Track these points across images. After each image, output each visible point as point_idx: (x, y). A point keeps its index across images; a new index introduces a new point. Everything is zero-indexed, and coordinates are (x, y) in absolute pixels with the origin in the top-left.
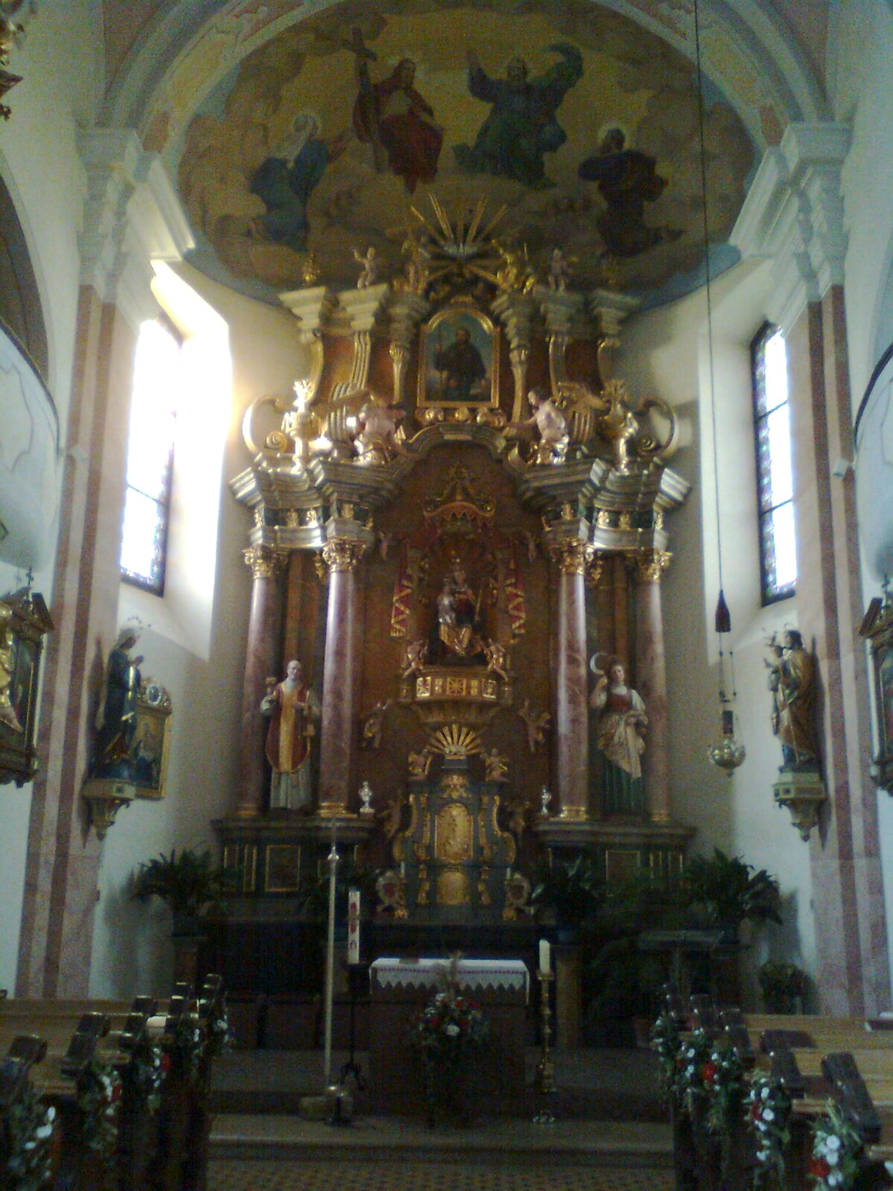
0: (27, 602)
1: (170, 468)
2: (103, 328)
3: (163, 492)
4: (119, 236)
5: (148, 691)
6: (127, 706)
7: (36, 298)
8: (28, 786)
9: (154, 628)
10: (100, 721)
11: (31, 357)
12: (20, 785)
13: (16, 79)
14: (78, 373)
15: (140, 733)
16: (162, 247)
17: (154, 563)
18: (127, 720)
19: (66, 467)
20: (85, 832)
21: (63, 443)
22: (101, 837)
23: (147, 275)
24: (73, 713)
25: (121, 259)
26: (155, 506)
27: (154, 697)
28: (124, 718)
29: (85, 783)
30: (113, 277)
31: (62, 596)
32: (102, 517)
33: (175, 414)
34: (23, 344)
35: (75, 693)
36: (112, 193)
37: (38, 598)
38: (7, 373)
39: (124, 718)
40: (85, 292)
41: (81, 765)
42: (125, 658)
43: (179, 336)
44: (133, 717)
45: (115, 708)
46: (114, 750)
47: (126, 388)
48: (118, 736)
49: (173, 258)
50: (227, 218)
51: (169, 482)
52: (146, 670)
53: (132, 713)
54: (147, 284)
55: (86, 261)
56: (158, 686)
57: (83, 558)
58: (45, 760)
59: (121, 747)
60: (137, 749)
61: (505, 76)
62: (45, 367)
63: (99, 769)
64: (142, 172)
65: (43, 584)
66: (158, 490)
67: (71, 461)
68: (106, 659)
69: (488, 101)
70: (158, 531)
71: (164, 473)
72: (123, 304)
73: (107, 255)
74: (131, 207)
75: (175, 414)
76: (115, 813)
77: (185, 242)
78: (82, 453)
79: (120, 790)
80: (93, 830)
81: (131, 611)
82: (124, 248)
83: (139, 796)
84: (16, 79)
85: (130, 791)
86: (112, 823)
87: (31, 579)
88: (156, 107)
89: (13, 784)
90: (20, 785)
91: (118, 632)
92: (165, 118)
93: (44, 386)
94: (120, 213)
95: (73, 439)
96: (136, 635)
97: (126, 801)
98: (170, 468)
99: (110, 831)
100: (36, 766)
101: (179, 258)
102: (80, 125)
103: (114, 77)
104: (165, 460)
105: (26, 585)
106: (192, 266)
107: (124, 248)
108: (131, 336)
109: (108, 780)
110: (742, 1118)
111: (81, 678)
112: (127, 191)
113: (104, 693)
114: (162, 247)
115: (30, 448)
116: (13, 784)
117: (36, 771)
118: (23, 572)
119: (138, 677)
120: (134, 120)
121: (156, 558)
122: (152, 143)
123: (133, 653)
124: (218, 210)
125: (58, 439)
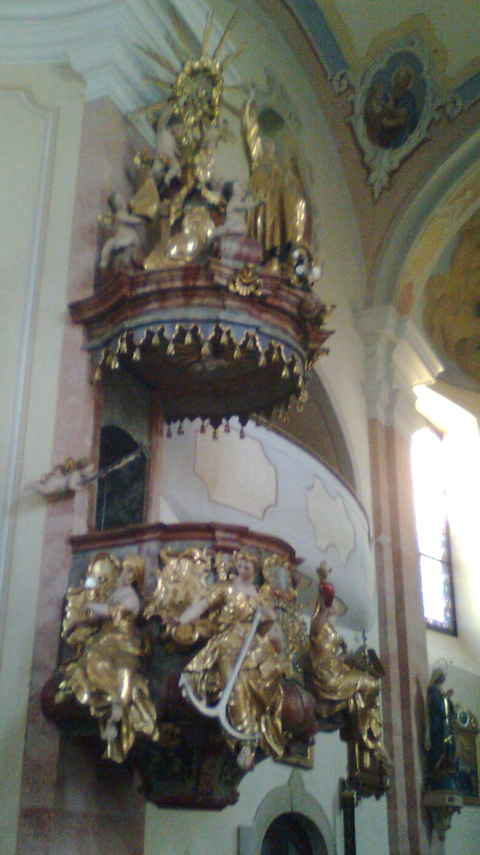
0: (365, 657)
1: (447, 534)
2: (388, 443)
3: (444, 554)
4: (390, 377)
5: (458, 716)
6: (446, 732)
7: (341, 435)
8: (384, 799)
9: (456, 664)
10: (428, 743)
11: (342, 477)
12: (378, 797)
13: (332, 332)
14: (375, 483)
15: (458, 751)
16: (420, 377)
17: (446, 610)
18: (448, 742)
19: (376, 552)
20: (430, 836)
21: (372, 535)
22: (442, 839)
23: (411, 399)
24: (407, 738)
25: (393, 395)
26: (440, 564)
27: (464, 720)
28: (446, 740)
29: (423, 794)
30: (390, 408)
31: (387, 649)
32: (407, 584)
33: (445, 492)
34: (337, 471)
35: (406, 724)
36: (381, 350)
37: (372, 652)
38: (334, 498)
39: (446, 740)
40: (372, 424)
41: (419, 779)
42: (439, 691)
43: (440, 434)
44: (452, 739)
45: (438, 732)
46: (441, 767)
47: (409, 484)
48: (443, 756)
49: (429, 382)
50: (463, 340)
51: (448, 544)
52: (454, 699)
53: (451, 736)
54: (413, 406)
55: (370, 402)
56: (465, 711)
57: (397, 617)
58: (393, 777)
59: (447, 764)
60: (457, 763)
61: (381, 108)
62: (354, 487)
63: (433, 782)
64: (400, 332)
65: (373, 643)
66: (440, 552)
67: (379, 547)
68: (425, 694)
69: (447, 692)
70: (445, 585)
71: (443, 538)
72: (399, 424)
73: (384, 395)
74: (396, 356)
75: (445, 492)
76: (450, 819)
77: (436, 368)
78: (386, 539)
79: (451, 800)
80: (435, 833)
81: (437, 652)
82: (395, 386)
83: (466, 803)
84: (332, 332)
85: (458, 800)
86: (449, 827)
87: (365, 639)
88: (403, 282)
89: (373, 798)
90: (378, 797)
91: (430, 672)
92: (410, 286)
93: (354, 495)
94: (389, 362)
95: (378, 531)
96: (445, 673)
97: (457, 809)
98: (447, 534)
99: (448, 834)
100: (388, 783)
101: (433, 381)
102: (355, 311)
103: (372, 272)
104: (443, 526)
105: (362, 644)
106: (444, 383)
107: (395, 386)
108: (407, 443)
109: (440, 791)
110: (126, 354)
111: (409, 710)
112: (391, 347)
113: (427, 723)
114: (420, 377)
115: (277, 501)
116: (373, 798)
117: (388, 788)
118: (360, 634)
119: (450, 703)
120: (388, 300)
121: (448, 606)
122: (403, 310)
123: (445, 687)
124: (456, 336)
125: (369, 534)
